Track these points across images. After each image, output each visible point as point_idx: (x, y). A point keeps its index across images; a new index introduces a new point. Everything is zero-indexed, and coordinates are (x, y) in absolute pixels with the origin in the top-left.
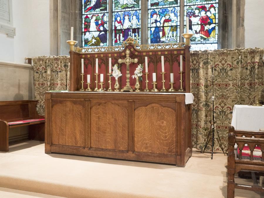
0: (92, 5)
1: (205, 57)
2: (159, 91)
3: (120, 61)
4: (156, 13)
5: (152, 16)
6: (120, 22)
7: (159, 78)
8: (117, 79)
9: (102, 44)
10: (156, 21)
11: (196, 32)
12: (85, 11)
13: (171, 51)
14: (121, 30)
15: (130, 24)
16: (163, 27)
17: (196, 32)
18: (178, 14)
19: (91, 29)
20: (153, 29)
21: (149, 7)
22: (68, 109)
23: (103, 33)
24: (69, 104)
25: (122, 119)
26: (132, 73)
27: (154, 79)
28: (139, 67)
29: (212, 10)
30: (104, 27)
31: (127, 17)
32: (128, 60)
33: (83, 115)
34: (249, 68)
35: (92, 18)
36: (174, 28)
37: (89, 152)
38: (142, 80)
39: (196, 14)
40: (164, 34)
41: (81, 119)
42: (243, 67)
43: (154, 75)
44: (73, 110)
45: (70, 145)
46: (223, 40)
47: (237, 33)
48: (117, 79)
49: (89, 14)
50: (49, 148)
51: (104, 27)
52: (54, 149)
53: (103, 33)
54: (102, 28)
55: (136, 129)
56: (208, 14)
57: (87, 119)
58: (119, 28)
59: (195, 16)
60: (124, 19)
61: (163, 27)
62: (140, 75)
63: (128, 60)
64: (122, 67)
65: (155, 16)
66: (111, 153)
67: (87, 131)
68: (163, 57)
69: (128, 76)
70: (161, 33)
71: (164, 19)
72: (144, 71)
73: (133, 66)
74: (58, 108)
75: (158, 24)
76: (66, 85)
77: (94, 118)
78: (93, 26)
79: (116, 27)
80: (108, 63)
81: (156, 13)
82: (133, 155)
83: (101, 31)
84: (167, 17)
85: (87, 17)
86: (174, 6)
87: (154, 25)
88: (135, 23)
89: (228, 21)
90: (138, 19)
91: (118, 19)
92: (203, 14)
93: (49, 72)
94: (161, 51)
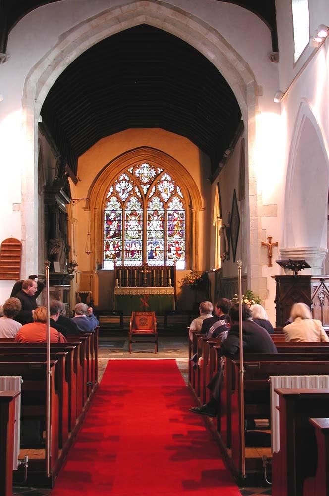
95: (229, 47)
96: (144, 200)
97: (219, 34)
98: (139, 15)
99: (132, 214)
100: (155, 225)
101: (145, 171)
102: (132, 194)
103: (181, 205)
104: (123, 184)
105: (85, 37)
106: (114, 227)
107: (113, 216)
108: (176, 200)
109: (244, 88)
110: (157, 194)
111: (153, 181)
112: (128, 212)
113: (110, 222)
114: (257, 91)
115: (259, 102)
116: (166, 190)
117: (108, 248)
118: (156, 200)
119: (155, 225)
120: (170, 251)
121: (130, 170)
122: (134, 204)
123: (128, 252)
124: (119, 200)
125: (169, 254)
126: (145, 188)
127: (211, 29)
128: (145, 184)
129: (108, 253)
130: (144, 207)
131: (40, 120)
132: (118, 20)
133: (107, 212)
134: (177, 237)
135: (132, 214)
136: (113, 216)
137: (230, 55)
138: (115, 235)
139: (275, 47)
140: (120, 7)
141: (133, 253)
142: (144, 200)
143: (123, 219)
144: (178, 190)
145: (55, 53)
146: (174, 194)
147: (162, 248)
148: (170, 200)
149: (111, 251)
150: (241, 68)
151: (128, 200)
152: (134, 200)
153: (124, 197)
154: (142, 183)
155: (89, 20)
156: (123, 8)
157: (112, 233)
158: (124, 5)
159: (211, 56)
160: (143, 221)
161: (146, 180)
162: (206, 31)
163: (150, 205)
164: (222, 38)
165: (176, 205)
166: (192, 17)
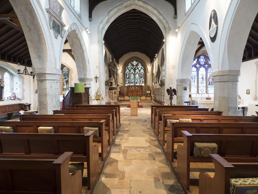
36: (139, 82)
46: (145, 84)
49: (127, 79)
67: (132, 94)
80: (39, 161)
88: (133, 81)
89: (106, 68)
95: (161, 14)
96: (135, 70)
97: (157, 10)
98: (132, 5)
99: (132, 73)
100: (137, 76)
101: (135, 63)
102: (132, 68)
103: (143, 71)
104: (130, 66)
105: (116, 13)
106: (128, 76)
107: (127, 74)
108: (142, 70)
109: (165, 28)
110: (138, 68)
111: (137, 65)
112: (131, 73)
113: (127, 75)
114: (170, 29)
115: (170, 33)
116: (140, 67)
117: (126, 81)
118: (137, 70)
119: (137, 76)
120: (141, 82)
121: (131, 62)
122: (132, 71)
123: (131, 82)
124: (129, 70)
125: (140, 83)
126: (135, 67)
127: (155, 9)
128: (135, 66)
129: (126, 82)
130: (135, 71)
131: (177, 156)
132: (126, 7)
133: (126, 73)
134: (142, 78)
135: (132, 73)
136: (127, 74)
137: (161, 18)
138: (128, 78)
139: (176, 13)
140: (126, 2)
141: (132, 82)
142: (135, 70)
143: (129, 74)
144: (143, 67)
145: (106, 18)
146: (142, 68)
147: (139, 81)
148: (141, 70)
149: (127, 82)
150: (164, 22)
151: (131, 70)
152: (132, 70)
153: (130, 69)
154: (134, 66)
155: (117, 7)
156: (127, 2)
157: (127, 78)
158: (128, 1)
159: (154, 18)
160: (135, 75)
161: (135, 65)
162: (153, 9)
163: (136, 71)
164: (159, 12)
165: (142, 71)
166: (149, 5)
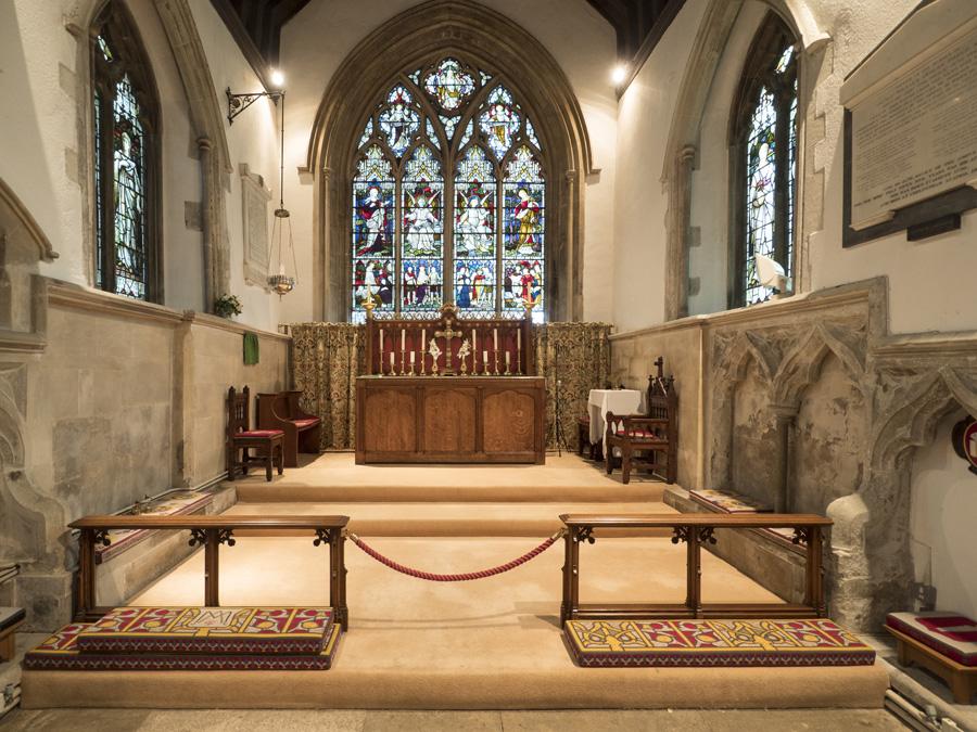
0: (369, 245)
1: (543, 331)
2: (398, 375)
3: (437, 333)
4: (464, 266)
5: (458, 269)
6: (412, 275)
7: (398, 359)
8: (436, 358)
9: (384, 306)
10: (464, 277)
11: (517, 296)
12: (358, 253)
13: (483, 323)
14: (414, 285)
15: (426, 278)
16: (474, 286)
17: (517, 296)
18: (495, 270)
19: (367, 282)
20: (460, 288)
21: (455, 257)
22: (390, 401)
23: (386, 288)
24: (392, 393)
25: (467, 410)
26: (455, 350)
27: (413, 360)
28: (466, 343)
29: (537, 267)
30: (387, 280)
31: (422, 269)
32: (449, 333)
33: (413, 409)
34: (593, 346)
35: (368, 265)
36: (489, 288)
37: (423, 457)
38: (469, 359)
39: (518, 272)
40: (475, 296)
41: (411, 413)
42: (586, 345)
43: (413, 354)
44: (398, 403)
45: (394, 449)
46: (552, 308)
47: (575, 302)
48: (436, 358)
50: (361, 456)
51: (387, 280)
52: (369, 457)
53: (386, 288)
54: (384, 282)
55: (486, 423)
56: (532, 272)
57: (418, 414)
58: (410, 283)
59: (516, 275)
60: (418, 270)
61: (474, 286)
62: (468, 353)
63: (449, 333)
64: (441, 342)
65: (463, 270)
66: (454, 456)
67: (418, 432)
68: (424, 331)
69: (449, 354)
70: (471, 295)
71: (475, 274)
72: (470, 350)
73: (457, 342)
74: (374, 402)
75: (467, 282)
76: (349, 368)
77: (429, 411)
78: (370, 277)
79: (405, 282)
81: (464, 266)
82: (484, 456)
83: (382, 286)
84: (480, 273)
85: (360, 263)
86: (488, 258)
87: (462, 282)
90: (438, 271)
91: (410, 269)
92: (525, 271)
93: (321, 347)
94: (421, 322)
